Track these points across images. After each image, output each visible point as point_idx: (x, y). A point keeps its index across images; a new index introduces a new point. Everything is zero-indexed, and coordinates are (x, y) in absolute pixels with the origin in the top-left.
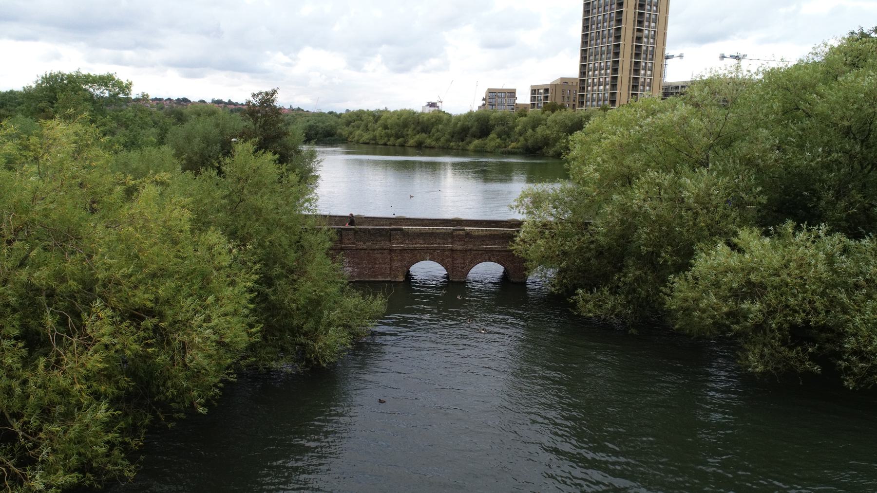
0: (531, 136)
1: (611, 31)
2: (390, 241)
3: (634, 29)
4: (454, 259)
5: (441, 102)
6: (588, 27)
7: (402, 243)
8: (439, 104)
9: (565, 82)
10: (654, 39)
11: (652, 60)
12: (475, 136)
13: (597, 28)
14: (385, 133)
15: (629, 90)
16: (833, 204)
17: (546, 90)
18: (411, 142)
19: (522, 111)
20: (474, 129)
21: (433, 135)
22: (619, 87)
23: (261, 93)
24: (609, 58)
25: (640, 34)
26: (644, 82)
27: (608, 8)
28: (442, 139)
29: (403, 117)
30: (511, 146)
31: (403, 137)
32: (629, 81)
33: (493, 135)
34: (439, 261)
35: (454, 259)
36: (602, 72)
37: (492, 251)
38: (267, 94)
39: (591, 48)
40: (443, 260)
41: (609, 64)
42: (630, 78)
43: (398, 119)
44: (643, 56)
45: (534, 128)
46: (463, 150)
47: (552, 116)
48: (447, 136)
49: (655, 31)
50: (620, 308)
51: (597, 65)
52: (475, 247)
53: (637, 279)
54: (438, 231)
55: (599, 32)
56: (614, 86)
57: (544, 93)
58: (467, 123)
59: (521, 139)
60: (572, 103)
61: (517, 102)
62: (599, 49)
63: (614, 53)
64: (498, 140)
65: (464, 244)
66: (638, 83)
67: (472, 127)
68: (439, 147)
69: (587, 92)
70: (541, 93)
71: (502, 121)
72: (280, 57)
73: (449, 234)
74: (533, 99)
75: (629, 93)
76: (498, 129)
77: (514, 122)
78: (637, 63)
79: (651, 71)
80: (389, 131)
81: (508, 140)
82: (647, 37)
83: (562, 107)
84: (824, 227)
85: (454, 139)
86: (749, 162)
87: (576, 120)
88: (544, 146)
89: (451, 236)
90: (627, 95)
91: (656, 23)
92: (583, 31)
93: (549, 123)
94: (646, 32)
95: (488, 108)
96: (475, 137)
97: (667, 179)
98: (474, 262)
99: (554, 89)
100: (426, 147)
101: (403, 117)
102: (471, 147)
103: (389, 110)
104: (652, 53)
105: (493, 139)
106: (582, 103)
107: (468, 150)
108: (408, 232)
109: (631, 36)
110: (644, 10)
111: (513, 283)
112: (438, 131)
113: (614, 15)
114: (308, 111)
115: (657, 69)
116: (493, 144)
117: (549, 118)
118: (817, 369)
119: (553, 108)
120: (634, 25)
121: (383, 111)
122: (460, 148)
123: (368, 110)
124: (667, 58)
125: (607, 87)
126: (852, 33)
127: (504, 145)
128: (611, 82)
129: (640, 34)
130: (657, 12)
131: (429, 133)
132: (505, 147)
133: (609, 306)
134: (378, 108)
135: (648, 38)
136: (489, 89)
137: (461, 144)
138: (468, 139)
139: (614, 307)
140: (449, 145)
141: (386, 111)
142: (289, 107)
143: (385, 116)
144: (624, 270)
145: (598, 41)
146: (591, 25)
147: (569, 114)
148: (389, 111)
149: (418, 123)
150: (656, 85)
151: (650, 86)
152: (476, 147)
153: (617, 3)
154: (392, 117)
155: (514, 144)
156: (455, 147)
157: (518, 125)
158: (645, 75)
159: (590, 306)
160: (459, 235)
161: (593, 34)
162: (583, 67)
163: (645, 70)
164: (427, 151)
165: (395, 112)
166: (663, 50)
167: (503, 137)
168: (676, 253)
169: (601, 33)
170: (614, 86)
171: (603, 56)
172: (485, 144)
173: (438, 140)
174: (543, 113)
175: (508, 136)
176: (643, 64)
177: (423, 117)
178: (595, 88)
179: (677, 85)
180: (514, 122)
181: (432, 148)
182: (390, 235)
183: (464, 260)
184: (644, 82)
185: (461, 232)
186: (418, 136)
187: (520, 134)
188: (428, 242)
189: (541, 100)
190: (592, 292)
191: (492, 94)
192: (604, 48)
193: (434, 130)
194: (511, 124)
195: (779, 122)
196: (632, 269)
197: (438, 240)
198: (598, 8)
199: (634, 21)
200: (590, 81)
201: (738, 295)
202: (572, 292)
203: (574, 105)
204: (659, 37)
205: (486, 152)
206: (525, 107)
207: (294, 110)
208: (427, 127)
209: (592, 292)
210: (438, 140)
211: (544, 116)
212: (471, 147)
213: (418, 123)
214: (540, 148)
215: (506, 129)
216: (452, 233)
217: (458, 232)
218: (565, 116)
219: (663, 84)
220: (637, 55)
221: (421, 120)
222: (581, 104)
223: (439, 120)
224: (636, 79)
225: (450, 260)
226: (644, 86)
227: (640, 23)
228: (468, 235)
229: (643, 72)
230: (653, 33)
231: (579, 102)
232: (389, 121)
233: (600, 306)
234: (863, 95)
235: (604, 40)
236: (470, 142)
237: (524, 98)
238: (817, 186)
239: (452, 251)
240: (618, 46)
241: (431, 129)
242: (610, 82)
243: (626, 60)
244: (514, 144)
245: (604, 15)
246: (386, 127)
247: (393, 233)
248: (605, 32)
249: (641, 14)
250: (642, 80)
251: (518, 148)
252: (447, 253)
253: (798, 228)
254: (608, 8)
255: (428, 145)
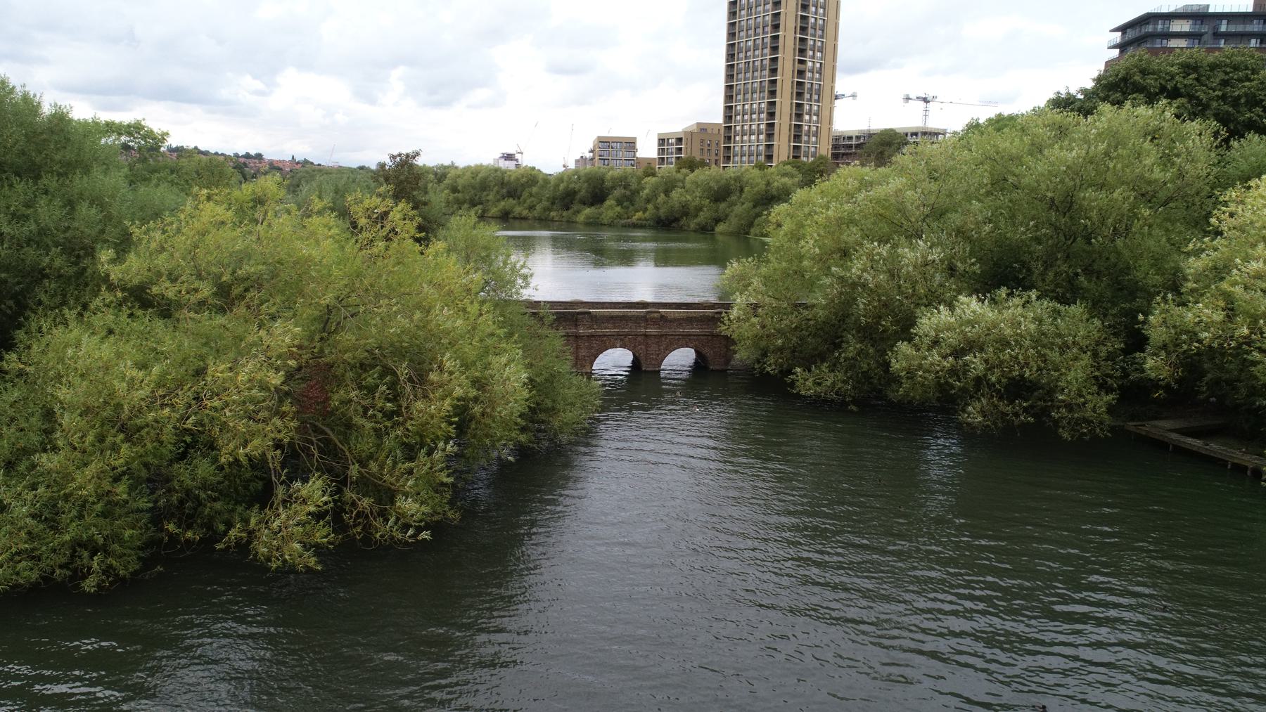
0: (664, 203)
1: (764, 62)
2: (576, 326)
3: (794, 60)
4: (647, 346)
5: (522, 153)
6: (733, 55)
7: (590, 328)
8: (518, 156)
9: (703, 128)
10: (820, 74)
11: (819, 102)
12: (584, 203)
13: (746, 58)
14: (454, 198)
15: (789, 141)
16: (1043, 274)
17: (679, 140)
18: (494, 211)
19: (649, 169)
20: (583, 193)
21: (525, 202)
22: (776, 136)
23: (400, 155)
24: (764, 98)
25: (802, 67)
26: (809, 131)
27: (760, 31)
28: (538, 207)
29: (480, 175)
30: (636, 217)
31: (482, 204)
32: (790, 130)
33: (608, 203)
34: (631, 348)
35: (647, 346)
36: (754, 116)
37: (690, 335)
38: (407, 156)
39: (738, 83)
40: (635, 347)
41: (763, 105)
42: (790, 125)
43: (473, 178)
44: (807, 96)
45: (667, 192)
46: (568, 221)
47: (692, 176)
48: (545, 203)
49: (821, 63)
50: (840, 385)
51: (746, 107)
52: (671, 331)
53: (860, 352)
54: (630, 314)
55: (749, 62)
56: (770, 136)
57: (677, 144)
58: (572, 186)
59: (650, 206)
60: (714, 158)
61: (638, 155)
62: (749, 86)
63: (769, 91)
64: (618, 209)
65: (659, 328)
66: (801, 131)
67: (579, 191)
68: (535, 218)
69: (734, 143)
70: (672, 144)
71: (623, 181)
72: (249, 82)
73: (642, 317)
74: (661, 151)
75: (789, 146)
76: (617, 192)
77: (639, 183)
78: (799, 106)
79: (818, 116)
80: (460, 195)
81: (631, 208)
82: (812, 71)
83: (703, 164)
84: (1033, 294)
85: (555, 207)
86: (960, 232)
87: (723, 182)
88: (682, 217)
89: (645, 320)
90: (787, 148)
91: (822, 52)
92: (728, 61)
93: (688, 185)
94: (810, 64)
95: (598, 163)
96: (584, 204)
97: (884, 250)
98: (670, 348)
99: (689, 140)
100: (515, 218)
101: (480, 175)
102: (581, 218)
103: (456, 165)
104: (819, 92)
105: (611, 207)
106: (729, 158)
107: (576, 222)
108: (596, 316)
109: (791, 69)
110: (807, 35)
111: (712, 370)
112: (531, 195)
113: (768, 40)
114: (319, 165)
115: (825, 113)
116: (611, 213)
117: (687, 178)
118: (1031, 419)
119: (692, 165)
120: (794, 55)
121: (448, 167)
122: (564, 219)
123: (424, 165)
124: (837, 98)
125: (762, 137)
126: (1058, 93)
127: (626, 216)
128: (766, 130)
129: (802, 67)
130: (823, 38)
131: (519, 199)
132: (628, 218)
133: (829, 383)
134: (440, 163)
135: (813, 73)
136: (599, 137)
137: (565, 213)
138: (575, 207)
139: (834, 384)
140: (549, 215)
141: (453, 166)
142: (290, 159)
143: (452, 173)
144: (844, 345)
145: (748, 75)
146: (738, 53)
147: (714, 174)
148: (456, 168)
149: (502, 184)
150: (824, 134)
151: (817, 137)
152: (588, 217)
153: (772, 25)
154: (464, 174)
155: (639, 214)
156: (557, 219)
157: (644, 188)
158: (810, 121)
159: (809, 383)
160: (654, 318)
161: (740, 66)
162: (728, 109)
163: (810, 115)
164: (517, 223)
165: (468, 168)
166: (832, 88)
167: (625, 204)
168: (897, 322)
169: (751, 64)
170: (770, 136)
171: (755, 96)
172: (601, 214)
173: (531, 208)
174: (678, 171)
175: (632, 203)
176: (807, 107)
177: (510, 176)
178: (745, 138)
179: (850, 134)
180: (639, 183)
181: (525, 219)
182: (577, 320)
183: (659, 346)
184: (809, 131)
185: (656, 315)
186: (503, 203)
187: (648, 201)
188: (618, 327)
189: (672, 153)
190: (810, 371)
191: (605, 144)
192: (755, 85)
193: (525, 194)
194: (634, 186)
195: (988, 193)
196: (853, 342)
197: (630, 324)
198: (747, 30)
199: (794, 49)
200: (738, 128)
201: (958, 353)
202: (789, 372)
203: (716, 160)
204: (827, 70)
205: (602, 224)
206: (649, 162)
207: (298, 163)
208: (516, 190)
209: (810, 371)
210: (531, 208)
211: (679, 176)
212: (581, 218)
213: (502, 184)
214: (677, 220)
215: (628, 193)
216: (645, 317)
217: (652, 315)
218: (709, 176)
219: (832, 134)
220: (800, 95)
221: (506, 179)
222: (728, 159)
223: (532, 181)
224: (798, 127)
225: (643, 347)
226: (809, 136)
227: (802, 52)
228: (663, 317)
229: (807, 117)
230: (818, 65)
231: (724, 157)
232: (461, 182)
233: (819, 384)
234: (1065, 168)
235: (756, 74)
236: (578, 212)
237: (647, 150)
238: (1026, 257)
239: (646, 336)
240: (774, 82)
241: (522, 192)
242: (764, 131)
243: (785, 102)
244: (639, 214)
245: (755, 40)
246: (454, 190)
247: (580, 317)
248: (756, 63)
249: (803, 40)
250: (806, 128)
251: (646, 220)
252: (639, 339)
253: (1010, 295)
254: (760, 31)
255: (518, 216)
